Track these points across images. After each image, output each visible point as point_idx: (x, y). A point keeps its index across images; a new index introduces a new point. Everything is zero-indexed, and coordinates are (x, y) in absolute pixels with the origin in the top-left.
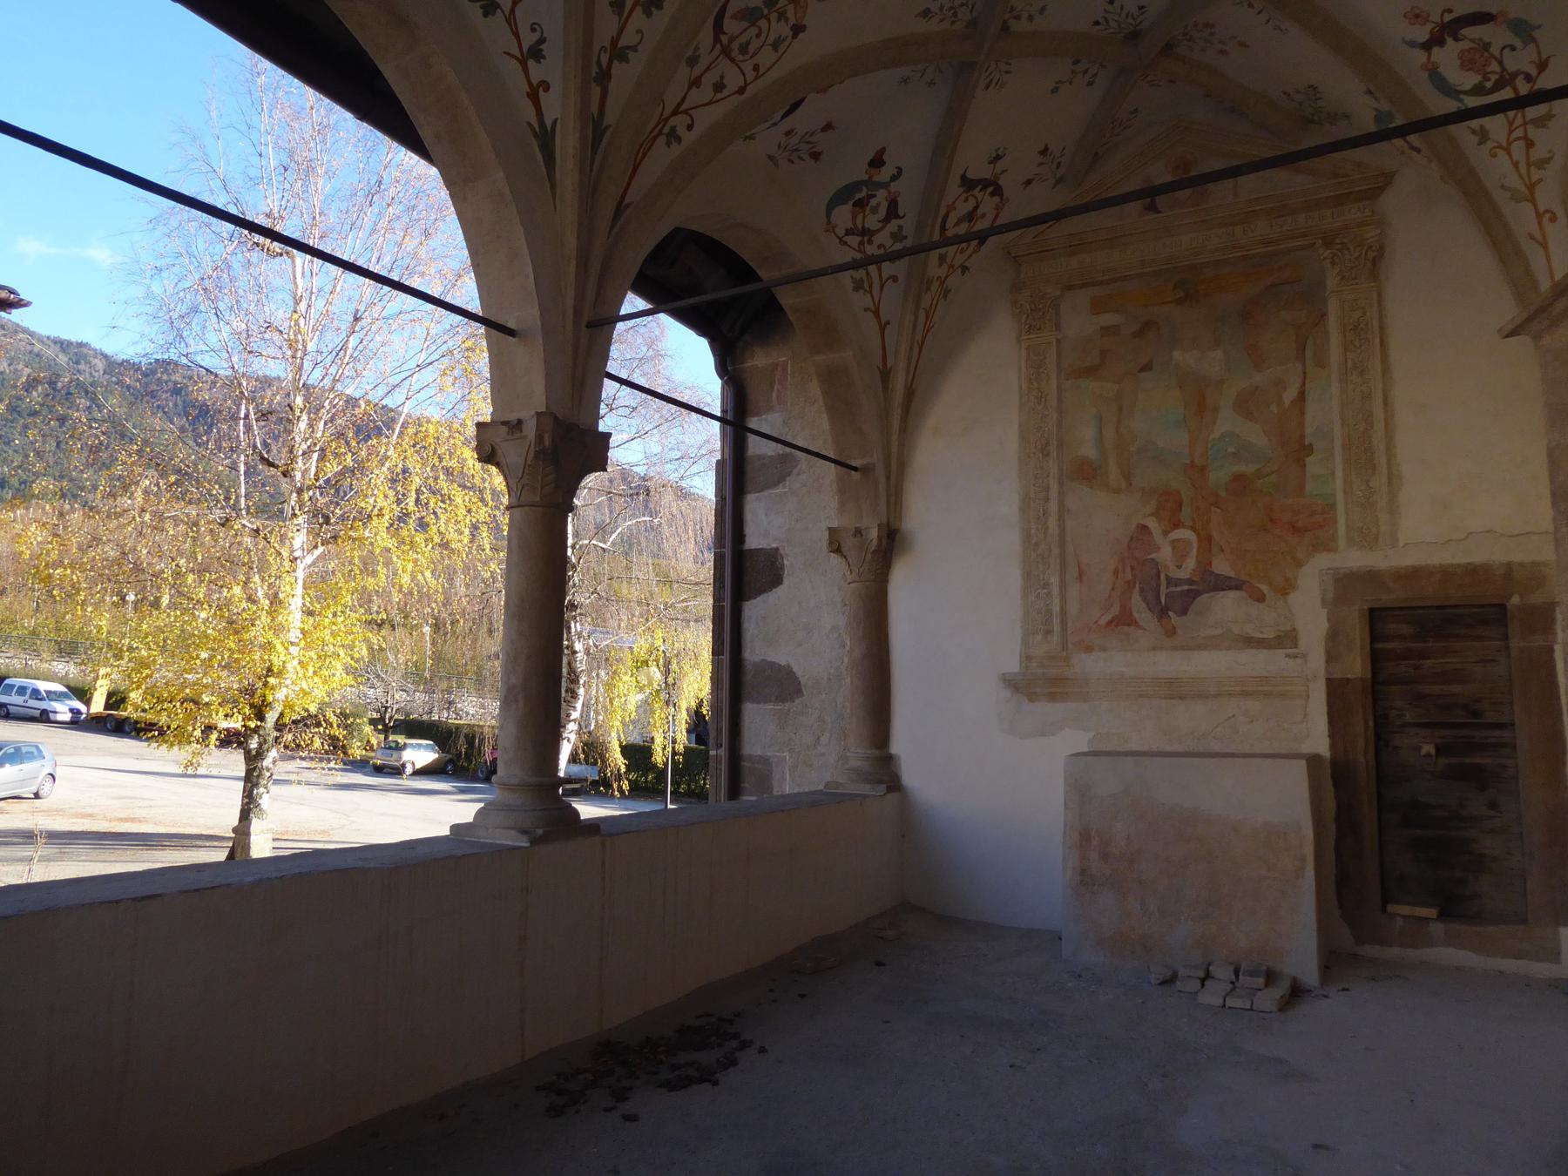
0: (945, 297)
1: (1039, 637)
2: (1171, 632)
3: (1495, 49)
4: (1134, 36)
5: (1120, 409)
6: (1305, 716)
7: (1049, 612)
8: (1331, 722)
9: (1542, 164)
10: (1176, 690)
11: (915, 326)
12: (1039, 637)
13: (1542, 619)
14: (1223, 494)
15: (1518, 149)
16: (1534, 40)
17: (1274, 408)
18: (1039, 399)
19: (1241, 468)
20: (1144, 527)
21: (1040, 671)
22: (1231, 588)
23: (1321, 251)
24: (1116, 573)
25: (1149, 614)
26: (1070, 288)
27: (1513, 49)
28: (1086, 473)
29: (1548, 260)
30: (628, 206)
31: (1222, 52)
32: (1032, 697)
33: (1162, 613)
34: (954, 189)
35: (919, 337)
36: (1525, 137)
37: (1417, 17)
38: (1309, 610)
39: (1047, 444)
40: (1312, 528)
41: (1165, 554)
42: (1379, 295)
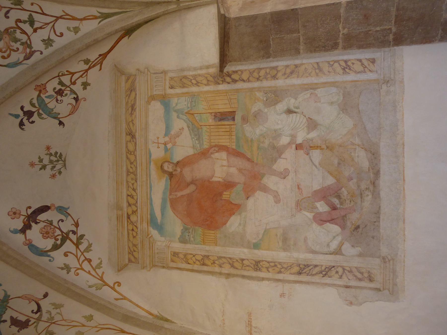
3: (55, 223)
9: (99, 266)
15: (86, 265)
16: (69, 214)
27: (62, 221)
29: (131, 301)
30: (49, 256)
36: (86, 259)
37: (14, 214)
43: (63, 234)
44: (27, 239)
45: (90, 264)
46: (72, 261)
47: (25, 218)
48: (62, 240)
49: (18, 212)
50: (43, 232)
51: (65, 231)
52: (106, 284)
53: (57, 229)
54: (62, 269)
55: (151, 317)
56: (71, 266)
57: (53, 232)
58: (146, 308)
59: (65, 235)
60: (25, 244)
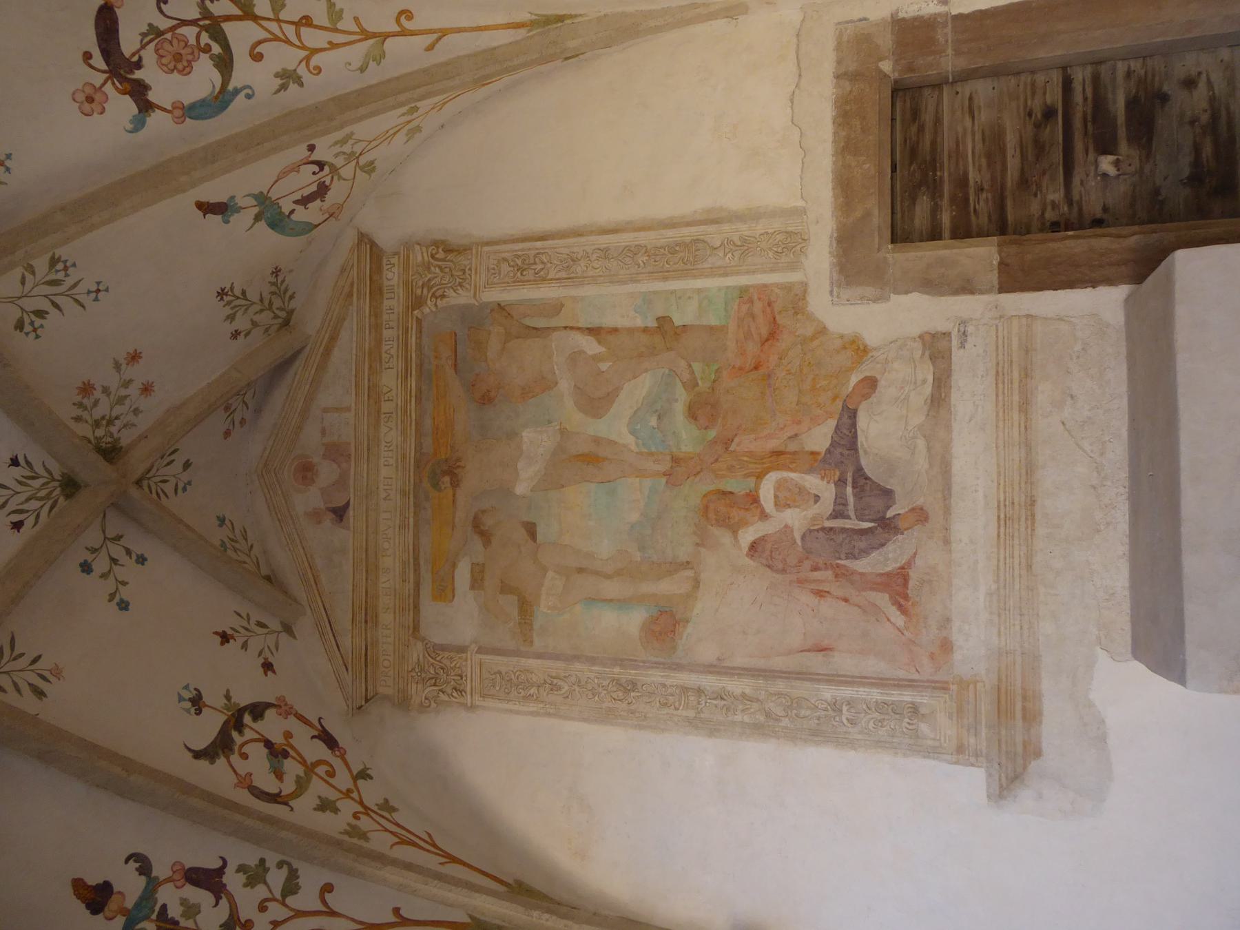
0: (393, 810)
1: (924, 728)
2: (920, 515)
4: (70, 486)
5: (581, 570)
6: (1060, 319)
7: (881, 706)
8: (1070, 285)
10: (1019, 512)
11: (409, 867)
12: (924, 728)
13: (913, 34)
14: (712, 434)
15: (312, 38)
17: (604, 366)
18: (555, 688)
19: (680, 408)
20: (754, 547)
21: (984, 732)
22: (854, 425)
23: (426, 310)
24: (820, 594)
25: (890, 547)
26: (416, 628)
28: (665, 626)
29: (459, 30)
30: (237, 92)
31: (147, 389)
32: (1033, 751)
33: (887, 526)
34: (218, 777)
35: (431, 861)
38: (891, 319)
39: (618, 682)
40: (771, 320)
41: (796, 519)
42: (488, 244)
43: (201, 23)
44: (169, 108)
45: (316, 27)
46: (281, 57)
47: (113, 83)
48: (213, 37)
49: (89, 90)
50: (171, 66)
51: (194, 14)
52: (385, 36)
53: (179, 31)
54: (284, 87)
55: (522, 32)
56: (291, 68)
57: (182, 44)
58: (501, 19)
59: (207, 22)
60: (180, 120)
